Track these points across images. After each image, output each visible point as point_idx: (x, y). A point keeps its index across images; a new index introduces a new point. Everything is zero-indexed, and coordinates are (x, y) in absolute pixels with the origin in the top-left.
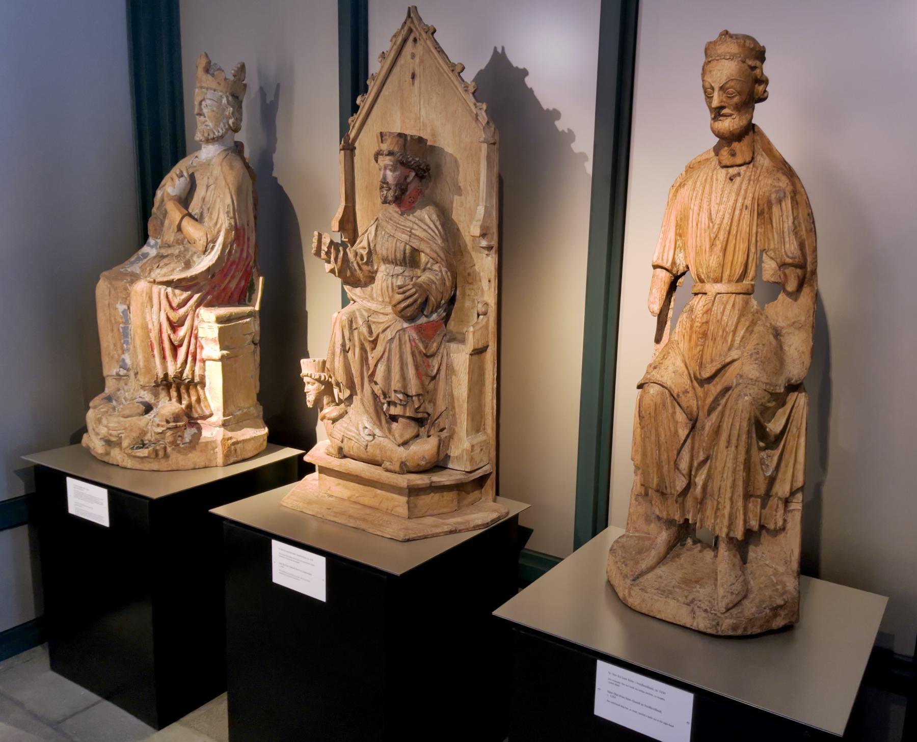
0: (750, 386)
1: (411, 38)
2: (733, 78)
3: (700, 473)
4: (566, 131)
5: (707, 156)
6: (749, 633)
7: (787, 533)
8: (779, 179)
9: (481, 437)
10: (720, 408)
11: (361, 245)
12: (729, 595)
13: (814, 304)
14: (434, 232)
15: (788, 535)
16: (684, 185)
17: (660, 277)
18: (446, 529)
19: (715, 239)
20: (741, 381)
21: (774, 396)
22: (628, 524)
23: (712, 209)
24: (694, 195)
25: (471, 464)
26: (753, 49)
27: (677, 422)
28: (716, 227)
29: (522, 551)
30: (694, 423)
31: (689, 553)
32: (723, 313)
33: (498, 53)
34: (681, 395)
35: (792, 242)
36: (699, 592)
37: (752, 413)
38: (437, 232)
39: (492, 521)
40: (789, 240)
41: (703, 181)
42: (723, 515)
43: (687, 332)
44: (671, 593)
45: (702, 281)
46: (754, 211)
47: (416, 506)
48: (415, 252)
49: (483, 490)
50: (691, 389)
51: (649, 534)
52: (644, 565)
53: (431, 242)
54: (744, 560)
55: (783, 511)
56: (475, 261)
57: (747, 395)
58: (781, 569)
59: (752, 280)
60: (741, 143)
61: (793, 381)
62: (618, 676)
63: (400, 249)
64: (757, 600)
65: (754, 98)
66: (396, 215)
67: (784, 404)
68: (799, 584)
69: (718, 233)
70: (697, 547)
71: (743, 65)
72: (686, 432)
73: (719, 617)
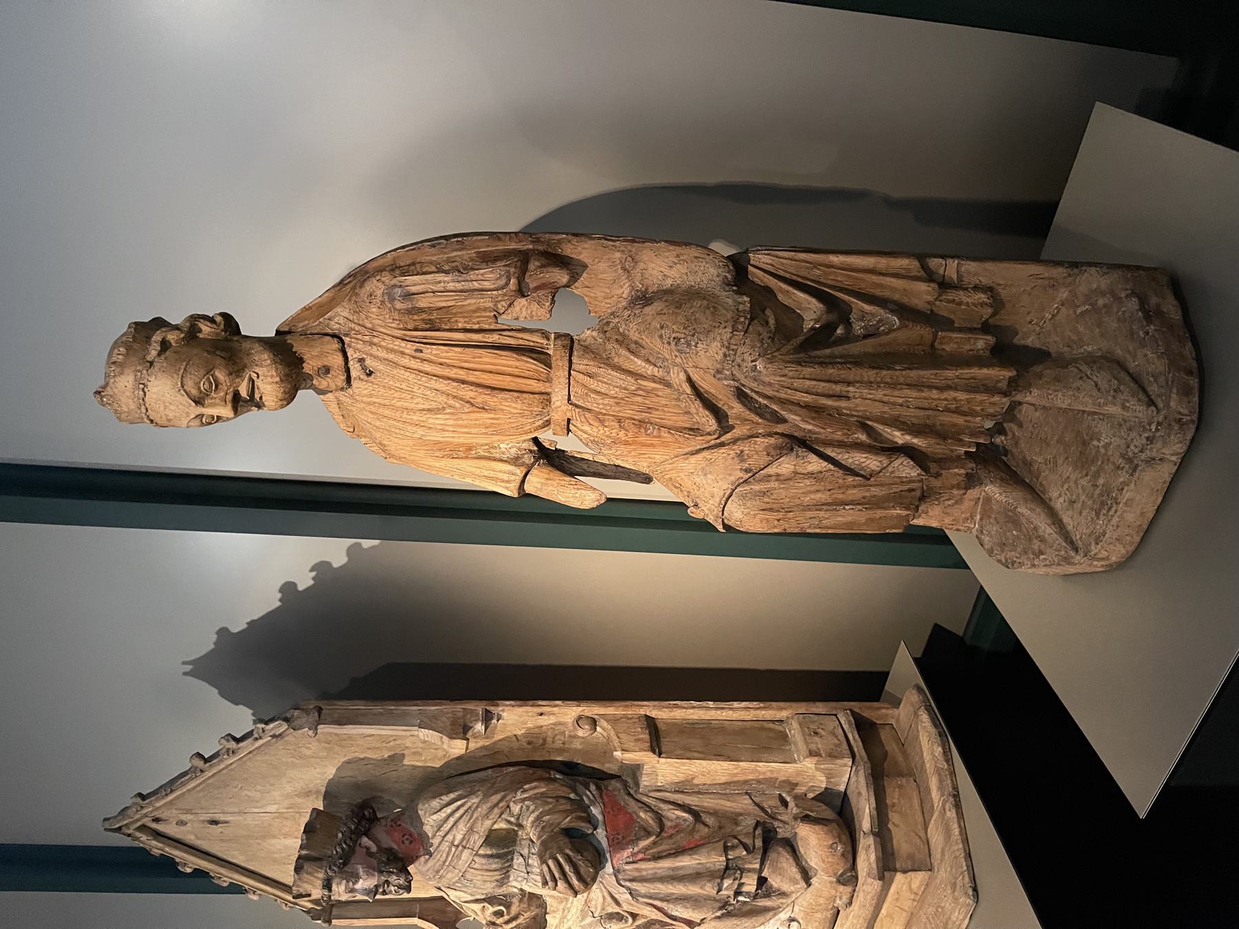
0: (738, 360)
1: (154, 826)
2: (179, 384)
3: (889, 437)
4: (313, 574)
5: (334, 407)
6: (1194, 364)
7: (999, 285)
9: (794, 731)
11: (479, 913)
12: (1121, 397)
14: (458, 808)
17: (539, 486)
18: (951, 814)
19: (472, 405)
21: (756, 314)
22: (958, 530)
23: (421, 407)
24: (398, 431)
25: (840, 756)
27: (796, 473)
28: (451, 402)
30: (799, 443)
33: (192, 670)
36: (1107, 446)
37: (787, 358)
38: (459, 803)
39: (936, 726)
42: (968, 401)
43: (635, 450)
46: (425, 338)
47: (911, 857)
48: (492, 839)
51: (979, 498)
52: (1047, 530)
53: (475, 816)
54: (1041, 356)
56: (509, 734)
57: (756, 365)
58: (1064, 294)
59: (548, 339)
60: (305, 357)
63: (485, 864)
65: (226, 340)
66: (431, 863)
67: (768, 290)
69: (461, 399)
70: (1011, 430)
71: (157, 366)
72: (813, 458)
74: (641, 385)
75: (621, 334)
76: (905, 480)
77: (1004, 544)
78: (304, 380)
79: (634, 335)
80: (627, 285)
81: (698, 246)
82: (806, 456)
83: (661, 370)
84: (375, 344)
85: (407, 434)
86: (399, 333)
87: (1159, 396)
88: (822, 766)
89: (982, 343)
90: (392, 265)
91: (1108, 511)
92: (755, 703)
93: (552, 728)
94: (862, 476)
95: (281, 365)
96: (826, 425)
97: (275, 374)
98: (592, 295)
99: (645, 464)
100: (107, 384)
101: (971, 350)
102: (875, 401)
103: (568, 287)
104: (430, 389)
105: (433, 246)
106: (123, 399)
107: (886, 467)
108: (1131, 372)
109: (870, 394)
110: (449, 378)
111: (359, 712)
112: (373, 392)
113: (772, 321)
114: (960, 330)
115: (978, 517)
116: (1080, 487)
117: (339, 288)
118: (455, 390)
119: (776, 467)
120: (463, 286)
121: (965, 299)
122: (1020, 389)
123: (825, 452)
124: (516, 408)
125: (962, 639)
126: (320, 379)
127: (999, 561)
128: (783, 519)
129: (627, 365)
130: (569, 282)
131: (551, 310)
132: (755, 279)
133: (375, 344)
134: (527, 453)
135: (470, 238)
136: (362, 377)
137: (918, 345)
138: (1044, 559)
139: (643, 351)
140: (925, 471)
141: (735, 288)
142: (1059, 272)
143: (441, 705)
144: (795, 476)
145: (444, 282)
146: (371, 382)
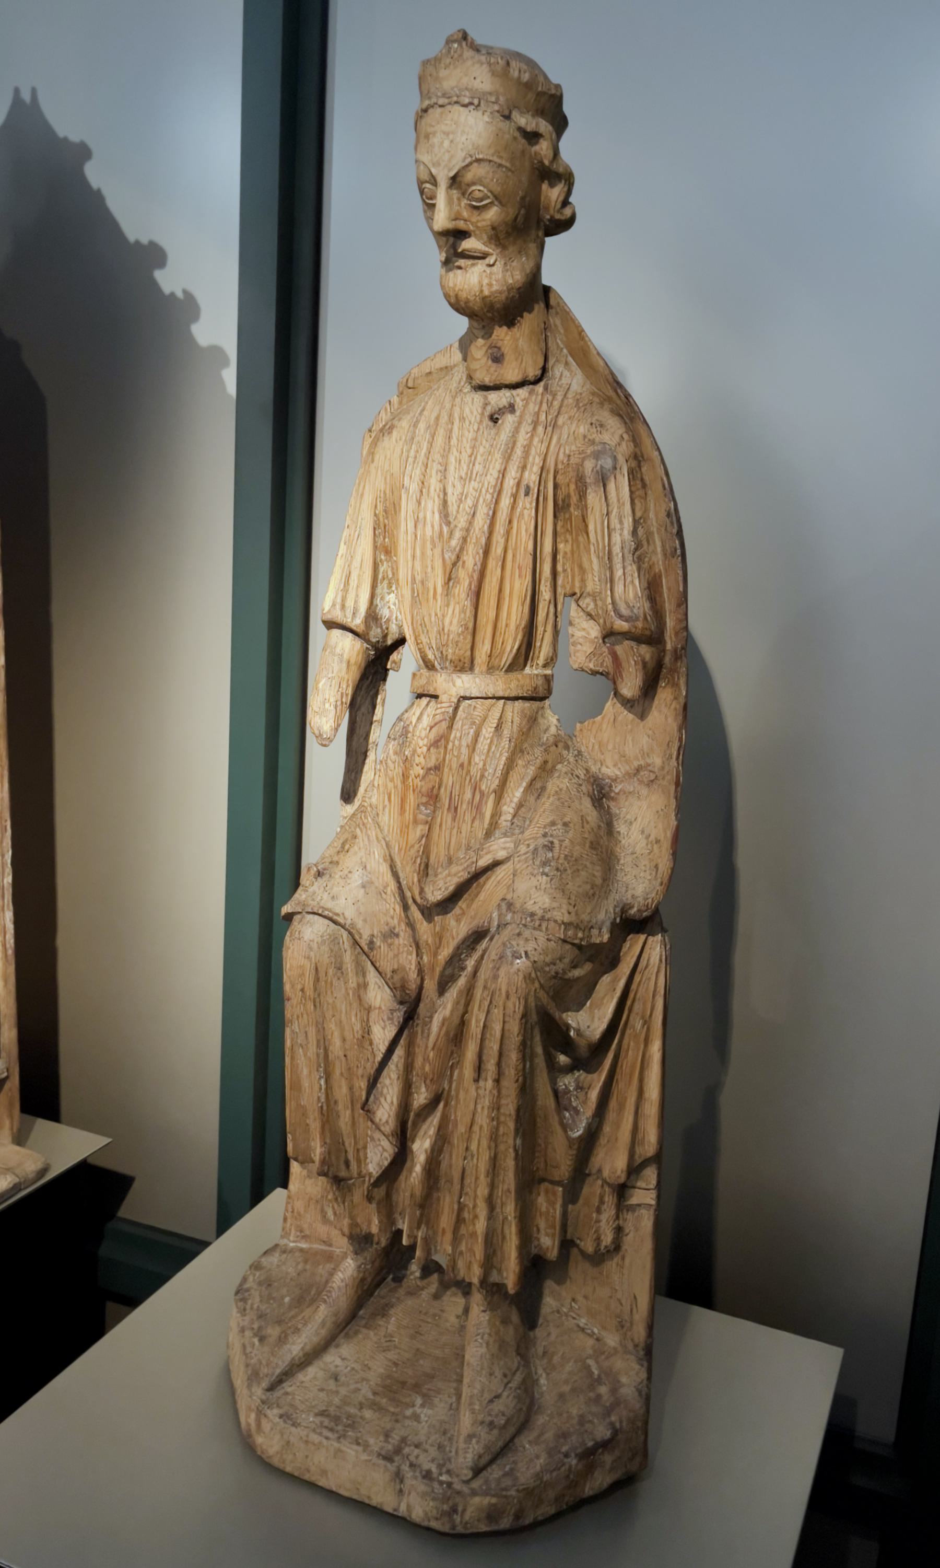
0: (527, 933)
2: (481, 156)
3: (421, 1132)
4: (180, 295)
5: (441, 362)
6: (528, 1520)
7: (623, 1258)
8: (601, 426)
10: (462, 982)
12: (483, 1432)
13: (680, 730)
16: (392, 428)
17: (338, 650)
20: (509, 917)
22: (285, 1219)
23: (450, 490)
24: (412, 453)
26: (528, 86)
27: (369, 1010)
28: (458, 534)
31: (410, 1302)
32: (473, 747)
34: (378, 942)
35: (629, 579)
36: (416, 1417)
40: (624, 574)
41: (432, 422)
42: (473, 1235)
43: (395, 787)
44: (352, 1426)
45: (429, 666)
46: (545, 499)
50: (403, 926)
51: (330, 1245)
52: (296, 1347)
55: (613, 1212)
58: (612, 1340)
60: (515, 329)
61: (633, 911)
64: (549, 1435)
65: (539, 220)
67: (613, 963)
69: (462, 549)
70: (428, 1285)
71: (505, 125)
72: (391, 1032)
74: (488, 797)
75: (554, 767)
76: (361, 1154)
77: (269, 1285)
79: (552, 785)
80: (618, 773)
83: (509, 824)
84: (534, 429)
85: (409, 468)
87: (486, 1482)
89: (548, 1243)
90: (643, 457)
91: (326, 1427)
92: (12, 941)
95: (507, 298)
98: (604, 726)
100: (478, 50)
101: (538, 1230)
102: (474, 1115)
104: (475, 506)
109: (483, 1108)
112: (467, 422)
113: (577, 973)
114: (565, 1214)
116: (359, 1386)
117: (610, 377)
118: (474, 541)
119: (376, 983)
120: (617, 555)
121: (604, 1217)
124: (451, 623)
126: (484, 349)
127: (245, 1279)
128: (304, 996)
129: (514, 777)
130: (621, 696)
131: (583, 670)
132: (627, 944)
133: (534, 429)
134: (383, 631)
135: (680, 566)
137: (546, 1161)
138: (254, 1345)
141: (618, 920)
142: (640, 1332)
144: (365, 1009)
145: (622, 529)
146: (481, 421)
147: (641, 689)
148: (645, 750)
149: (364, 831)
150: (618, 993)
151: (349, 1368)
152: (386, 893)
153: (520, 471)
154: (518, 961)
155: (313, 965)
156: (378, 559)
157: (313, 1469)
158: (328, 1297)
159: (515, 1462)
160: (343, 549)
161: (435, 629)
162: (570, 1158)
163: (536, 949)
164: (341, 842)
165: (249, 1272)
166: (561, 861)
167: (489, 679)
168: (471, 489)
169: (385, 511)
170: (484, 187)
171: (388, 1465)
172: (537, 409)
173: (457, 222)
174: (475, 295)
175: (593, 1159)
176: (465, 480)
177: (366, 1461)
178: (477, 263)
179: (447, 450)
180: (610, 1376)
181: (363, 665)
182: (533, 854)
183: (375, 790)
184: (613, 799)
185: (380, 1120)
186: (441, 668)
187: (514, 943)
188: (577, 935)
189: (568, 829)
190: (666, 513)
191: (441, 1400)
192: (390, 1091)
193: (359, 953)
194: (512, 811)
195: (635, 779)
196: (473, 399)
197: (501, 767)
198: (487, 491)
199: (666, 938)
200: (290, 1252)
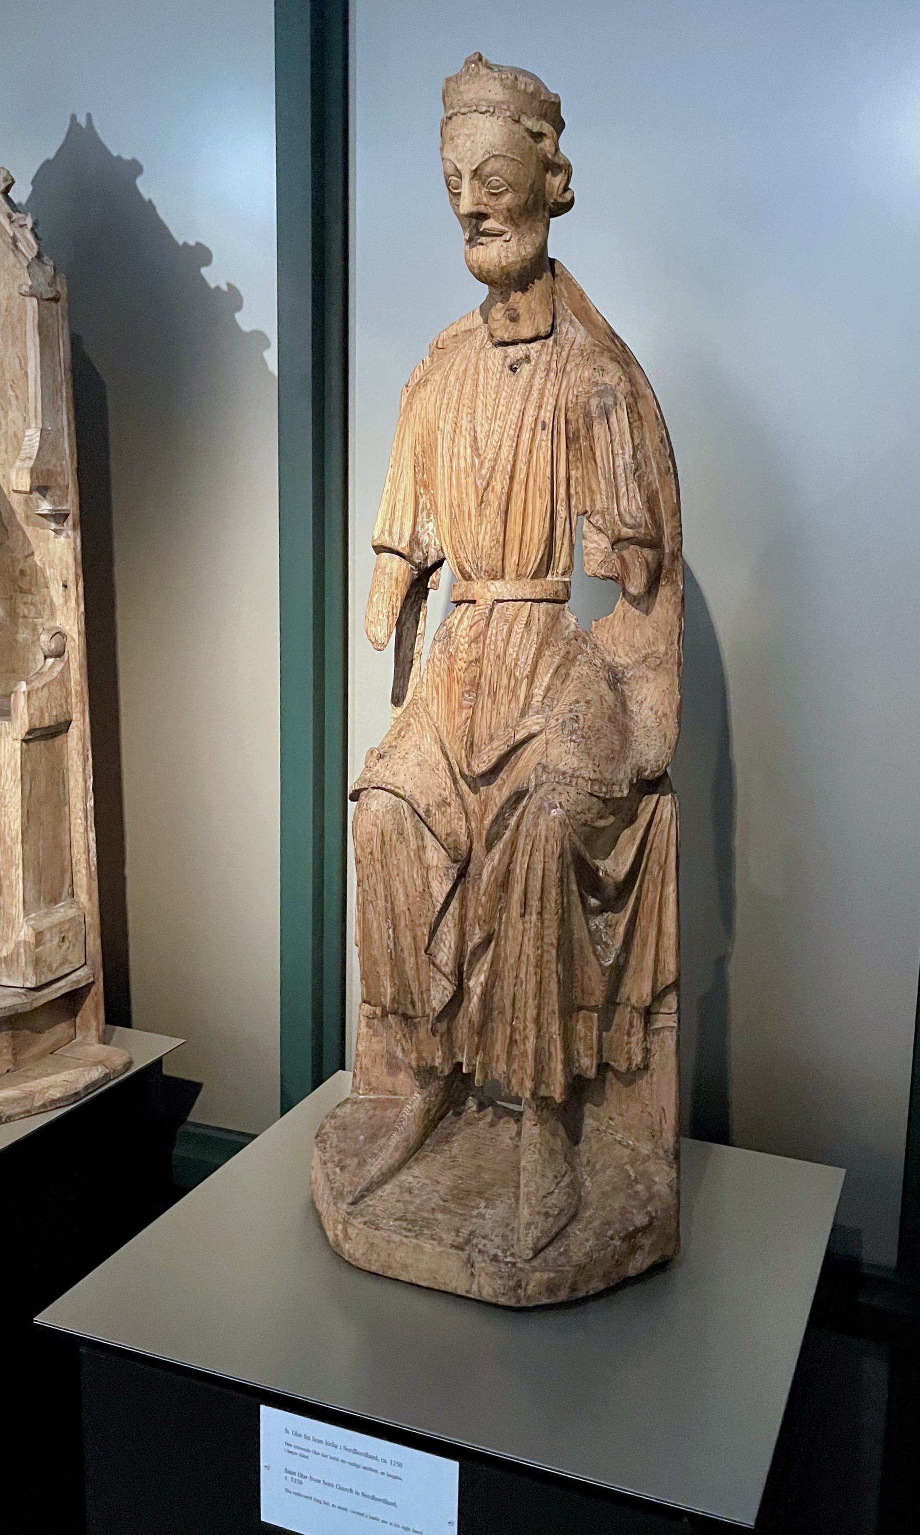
2: (497, 153)
3: (476, 971)
4: (225, 288)
5: (465, 325)
6: (581, 1294)
7: (651, 1076)
8: (603, 370)
9: (63, 912)
10: (508, 833)
12: (540, 1219)
15: (655, 1078)
16: (426, 381)
17: (388, 570)
19: (485, 489)
23: (478, 429)
24: (445, 401)
27: (428, 869)
28: (487, 465)
29: (181, 1129)
33: (79, 125)
35: (631, 495)
37: (566, 842)
39: (87, 1088)
42: (524, 1054)
43: (442, 680)
44: (428, 1226)
45: (467, 577)
46: (559, 433)
49: (78, 1019)
50: (454, 796)
51: (395, 1094)
52: (374, 1168)
54: (574, 1136)
55: (641, 1034)
56: (34, 546)
57: (556, 807)
58: (645, 1149)
59: (563, 574)
60: (528, 294)
62: (306, 1437)
64: (596, 1223)
65: (545, 204)
67: (632, 820)
68: (678, 1177)
69: (491, 477)
70: (484, 1116)
71: (516, 127)
72: (447, 887)
73: (521, 1269)
74: (522, 682)
75: (575, 657)
76: (425, 996)
78: (502, 292)
79: (574, 673)
80: (629, 661)
81: (679, 735)
82: (448, 878)
83: (540, 704)
84: (547, 375)
85: (443, 413)
86: (562, 401)
88: (22, 950)
89: (587, 1064)
90: (638, 394)
92: (95, 859)
93: (45, 600)
94: (429, 944)
95: (521, 268)
96: (490, 895)
97: (510, 260)
98: (616, 622)
99: (424, 694)
101: (578, 1053)
102: (521, 946)
103: (624, 594)
104: (501, 440)
105: (662, 441)
106: (475, 87)
107: (440, 971)
108: (568, 1228)
109: (529, 939)
110: (515, 461)
111: (56, 348)
112: (491, 373)
115: (372, 1097)
116: (430, 1196)
117: (608, 331)
118: (501, 468)
119: (433, 846)
120: (621, 474)
122: (539, 1113)
123: (454, 900)
124: (484, 539)
125: (183, 1120)
126: (503, 311)
127: (322, 1127)
131: (596, 576)
132: (644, 803)
133: (547, 375)
134: (424, 554)
136: (508, 360)
139: (558, 683)
140: (438, 1016)
141: (635, 781)
143: (72, 455)
144: (424, 867)
145: (623, 454)
146: (502, 372)
147: (646, 586)
148: (651, 640)
149: (417, 719)
150: (638, 841)
151: (420, 1184)
152: (438, 770)
153: (537, 410)
154: (554, 810)
155: (380, 831)
156: (418, 493)
157: (394, 1265)
158: (400, 1126)
159: (568, 1245)
160: (388, 485)
161: (471, 545)
162: (603, 984)
163: (568, 801)
164: (397, 730)
165: (325, 1121)
166: (585, 730)
167: (518, 584)
168: (497, 426)
169: (423, 452)
170: (501, 177)
171: (460, 1253)
172: (548, 359)
173: (479, 206)
174: (495, 266)
175: (622, 990)
176: (491, 420)
177: (442, 1252)
178: (495, 240)
179: (475, 395)
180: (645, 1177)
181: (409, 584)
182: (562, 726)
183: (424, 687)
184: (625, 683)
185: (441, 962)
186: (477, 578)
187: (550, 797)
188: (601, 789)
189: (590, 705)
190: (659, 440)
191: (502, 1201)
192: (448, 937)
193: (418, 821)
194: (542, 693)
195: (644, 665)
196: (495, 353)
197: (532, 656)
198: (510, 427)
199: (676, 798)
200: (360, 1103)
